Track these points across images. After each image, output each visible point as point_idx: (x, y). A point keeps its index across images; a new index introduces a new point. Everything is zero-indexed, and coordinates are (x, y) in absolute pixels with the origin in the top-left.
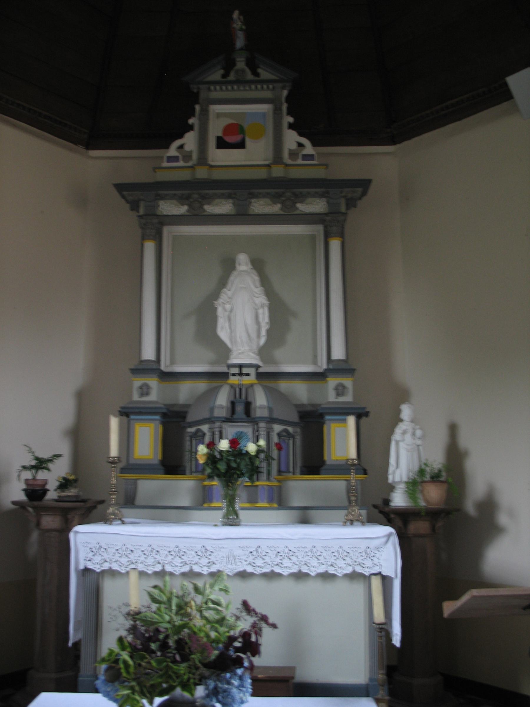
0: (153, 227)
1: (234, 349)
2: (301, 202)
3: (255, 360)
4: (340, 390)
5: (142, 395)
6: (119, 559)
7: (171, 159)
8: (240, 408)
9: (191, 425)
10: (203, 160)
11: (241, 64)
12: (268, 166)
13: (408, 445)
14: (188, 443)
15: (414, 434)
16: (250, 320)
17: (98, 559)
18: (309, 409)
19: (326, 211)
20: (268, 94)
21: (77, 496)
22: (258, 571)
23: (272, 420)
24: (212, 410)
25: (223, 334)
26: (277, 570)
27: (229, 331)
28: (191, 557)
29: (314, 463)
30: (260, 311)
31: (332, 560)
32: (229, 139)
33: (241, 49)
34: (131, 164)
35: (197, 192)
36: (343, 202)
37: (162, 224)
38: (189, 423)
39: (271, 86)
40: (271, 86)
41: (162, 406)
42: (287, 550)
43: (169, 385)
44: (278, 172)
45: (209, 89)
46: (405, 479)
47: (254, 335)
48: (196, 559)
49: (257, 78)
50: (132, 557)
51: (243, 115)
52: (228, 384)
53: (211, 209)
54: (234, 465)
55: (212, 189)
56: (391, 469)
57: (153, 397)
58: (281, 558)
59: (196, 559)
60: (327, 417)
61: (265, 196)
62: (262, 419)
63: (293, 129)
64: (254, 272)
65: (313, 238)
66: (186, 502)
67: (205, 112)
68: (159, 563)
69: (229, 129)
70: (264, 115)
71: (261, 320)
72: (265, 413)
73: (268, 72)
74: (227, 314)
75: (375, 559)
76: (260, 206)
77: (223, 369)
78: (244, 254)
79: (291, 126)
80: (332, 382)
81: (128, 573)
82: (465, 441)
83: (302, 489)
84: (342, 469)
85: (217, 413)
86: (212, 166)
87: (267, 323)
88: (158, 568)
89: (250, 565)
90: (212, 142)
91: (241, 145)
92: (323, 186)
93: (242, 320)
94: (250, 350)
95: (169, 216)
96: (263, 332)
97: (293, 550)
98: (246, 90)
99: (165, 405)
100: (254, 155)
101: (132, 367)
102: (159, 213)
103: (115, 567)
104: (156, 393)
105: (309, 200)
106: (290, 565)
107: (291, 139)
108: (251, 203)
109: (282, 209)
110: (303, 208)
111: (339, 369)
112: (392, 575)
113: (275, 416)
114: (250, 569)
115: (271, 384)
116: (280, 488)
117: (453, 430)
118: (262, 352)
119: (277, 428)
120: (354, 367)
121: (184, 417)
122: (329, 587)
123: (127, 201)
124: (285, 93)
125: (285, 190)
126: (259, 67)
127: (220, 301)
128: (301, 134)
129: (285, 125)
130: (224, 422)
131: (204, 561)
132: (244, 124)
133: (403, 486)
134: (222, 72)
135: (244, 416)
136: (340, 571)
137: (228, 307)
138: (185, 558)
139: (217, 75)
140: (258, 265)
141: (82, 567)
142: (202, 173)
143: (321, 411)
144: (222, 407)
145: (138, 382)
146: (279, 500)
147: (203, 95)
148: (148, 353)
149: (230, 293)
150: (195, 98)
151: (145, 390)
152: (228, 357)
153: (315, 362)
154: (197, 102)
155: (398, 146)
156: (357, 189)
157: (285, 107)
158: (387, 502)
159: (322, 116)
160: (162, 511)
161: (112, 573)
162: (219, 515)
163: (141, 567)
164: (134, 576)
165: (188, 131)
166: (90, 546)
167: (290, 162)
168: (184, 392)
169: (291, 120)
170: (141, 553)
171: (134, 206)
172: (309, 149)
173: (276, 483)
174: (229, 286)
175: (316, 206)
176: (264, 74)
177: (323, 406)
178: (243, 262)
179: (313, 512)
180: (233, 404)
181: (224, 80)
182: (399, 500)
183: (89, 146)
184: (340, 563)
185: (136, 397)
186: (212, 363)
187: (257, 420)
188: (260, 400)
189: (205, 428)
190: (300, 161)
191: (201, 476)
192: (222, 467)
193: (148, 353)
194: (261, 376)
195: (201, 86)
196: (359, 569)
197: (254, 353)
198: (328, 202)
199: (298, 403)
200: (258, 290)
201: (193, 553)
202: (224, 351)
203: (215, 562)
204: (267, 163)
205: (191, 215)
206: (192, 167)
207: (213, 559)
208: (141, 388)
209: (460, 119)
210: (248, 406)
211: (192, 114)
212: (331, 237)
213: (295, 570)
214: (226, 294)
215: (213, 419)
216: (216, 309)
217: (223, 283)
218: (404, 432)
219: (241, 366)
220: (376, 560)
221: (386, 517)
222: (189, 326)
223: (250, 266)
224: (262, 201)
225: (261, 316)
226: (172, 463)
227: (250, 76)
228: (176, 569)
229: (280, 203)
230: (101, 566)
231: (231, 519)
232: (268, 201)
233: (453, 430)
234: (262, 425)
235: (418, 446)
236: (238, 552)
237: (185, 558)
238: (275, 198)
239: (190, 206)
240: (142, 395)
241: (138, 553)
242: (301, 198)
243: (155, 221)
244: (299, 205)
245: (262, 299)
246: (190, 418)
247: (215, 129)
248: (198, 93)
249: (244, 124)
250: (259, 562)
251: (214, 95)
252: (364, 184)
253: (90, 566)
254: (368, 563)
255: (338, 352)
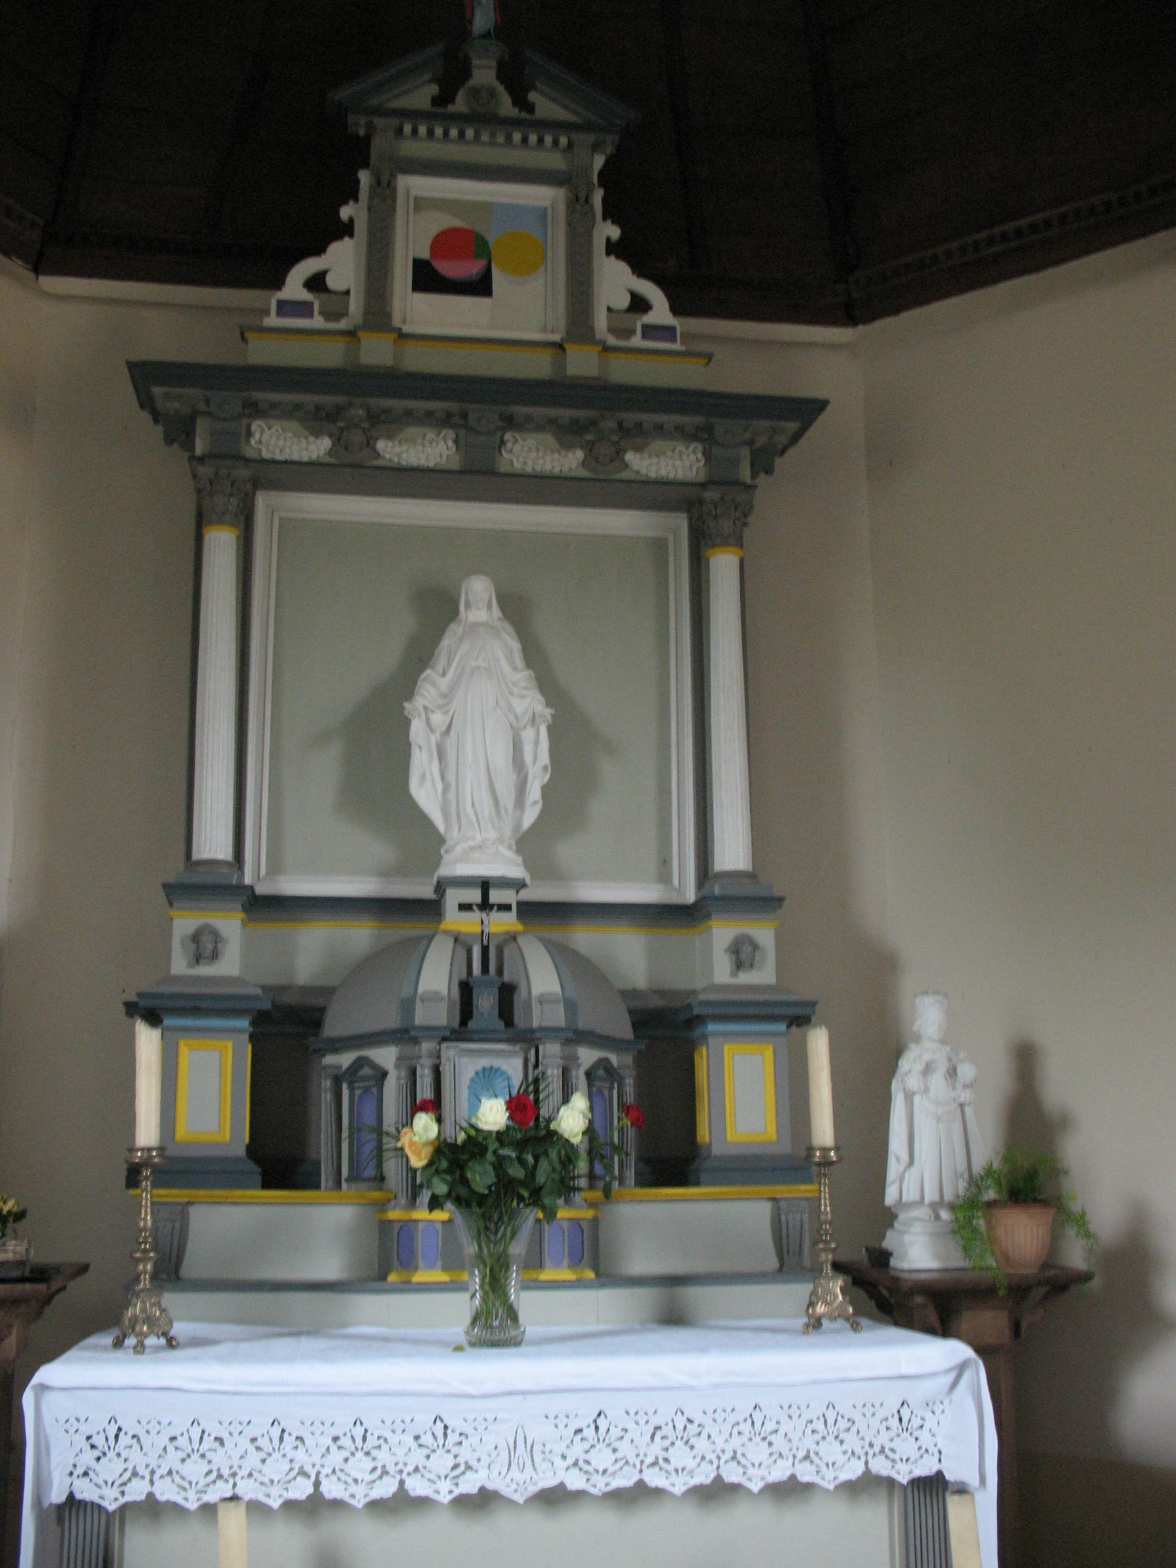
0: (229, 489)
1: (453, 836)
2: (638, 449)
3: (515, 870)
4: (743, 954)
5: (198, 959)
6: (177, 1466)
7: (286, 308)
8: (486, 1003)
9: (339, 1045)
10: (378, 314)
11: (484, 74)
12: (560, 346)
13: (938, 1104)
14: (327, 1097)
15: (952, 1073)
16: (501, 758)
17: (110, 1469)
18: (656, 1002)
19: (702, 478)
20: (555, 161)
21: (20, 1264)
22: (599, 1485)
23: (576, 1036)
24: (408, 1005)
25: (425, 792)
26: (654, 1479)
27: (439, 786)
28: (400, 1452)
29: (670, 1153)
30: (528, 735)
31: (809, 1442)
32: (450, 269)
33: (486, 35)
34: (170, 318)
35: (358, 401)
36: (745, 453)
37: (257, 484)
38: (332, 1041)
39: (563, 141)
40: (563, 141)
41: (259, 991)
42: (680, 1422)
43: (270, 931)
44: (582, 363)
45: (400, 131)
46: (931, 1195)
47: (508, 799)
48: (417, 1457)
49: (524, 115)
50: (220, 1459)
51: (487, 208)
52: (446, 932)
53: (394, 450)
54: (516, 1172)
55: (401, 397)
56: (893, 1169)
57: (229, 965)
58: (667, 1443)
59: (417, 1457)
60: (711, 1027)
61: (541, 427)
62: (551, 1032)
63: (619, 256)
64: (509, 627)
65: (659, 547)
66: (330, 1268)
67: (385, 190)
68: (303, 1473)
69: (446, 242)
70: (542, 215)
71: (528, 758)
72: (557, 1017)
73: (554, 100)
74: (434, 739)
75: (924, 1435)
76: (527, 453)
77: (426, 891)
78: (482, 577)
79: (612, 249)
80: (722, 932)
81: (209, 1510)
82: (1059, 1087)
83: (651, 1225)
84: (750, 1169)
85: (422, 1016)
86: (402, 336)
87: (545, 768)
88: (301, 1490)
89: (576, 1470)
90: (402, 275)
91: (481, 287)
92: (704, 413)
93: (478, 759)
94: (500, 840)
95: (280, 462)
96: (534, 792)
97: (698, 1418)
98: (499, 145)
99: (264, 988)
100: (516, 315)
101: (171, 879)
102: (250, 453)
103: (166, 1492)
104: (239, 954)
105: (658, 444)
106: (691, 1464)
107: (615, 281)
108: (503, 442)
109: (584, 464)
110: (645, 464)
111: (716, 897)
112: (973, 1480)
113: (582, 1024)
114: (575, 1482)
115: (557, 934)
116: (595, 1221)
117: (1026, 1060)
118: (528, 844)
119: (587, 1056)
120: (778, 892)
121: (317, 1024)
122: (795, 1519)
123: (157, 417)
124: (599, 161)
125: (600, 413)
126: (534, 88)
127: (419, 702)
128: (639, 270)
129: (599, 246)
130: (445, 1039)
131: (442, 1463)
132: (486, 232)
133: (923, 1212)
134: (434, 89)
135: (500, 1025)
136: (829, 1474)
137: (438, 719)
138: (383, 1456)
139: (421, 96)
140: (515, 609)
141: (57, 1496)
142: (376, 351)
143: (696, 1011)
144: (435, 997)
145: (185, 923)
146: (596, 1261)
147: (378, 145)
148: (213, 841)
149: (444, 683)
150: (358, 152)
151: (205, 946)
152: (437, 861)
153: (664, 877)
154: (366, 165)
155: (861, 328)
156: (783, 424)
157: (598, 196)
158: (881, 1258)
159: (692, 227)
160: (272, 1301)
161: (153, 1509)
162: (458, 1309)
163: (248, 1490)
164: (233, 1521)
165: (339, 237)
166: (86, 1429)
167: (612, 340)
168: (310, 954)
169: (615, 232)
170: (251, 1448)
171: (179, 431)
172: (661, 312)
173: (589, 1214)
174: (442, 662)
175: (675, 462)
176: (546, 106)
177: (703, 997)
178: (479, 598)
179: (695, 1294)
180: (466, 989)
181: (441, 110)
182: (918, 1252)
183: (39, 265)
184: (831, 1451)
185: (179, 965)
186: (385, 873)
187: (538, 1035)
188: (541, 978)
189: (386, 1056)
190: (637, 341)
191: (377, 1195)
192: (481, 1177)
193: (213, 841)
194: (531, 911)
195: (378, 122)
196: (880, 1467)
197: (509, 848)
198: (707, 455)
199: (629, 986)
200: (522, 677)
201: (408, 1439)
202: (421, 839)
203: (473, 1463)
204: (556, 338)
205: (335, 465)
206: (351, 334)
207: (465, 1454)
208: (196, 937)
209: (1037, 269)
210: (507, 993)
211: (352, 194)
212: (714, 546)
213: (704, 1476)
214: (434, 684)
215: (413, 1033)
216: (407, 723)
217: (420, 655)
218: (928, 1069)
219: (485, 885)
220: (925, 1438)
221: (871, 1296)
222: (323, 772)
223: (496, 612)
224: (531, 440)
225: (528, 750)
226: (278, 1158)
227: (506, 107)
228: (353, 1489)
229: (582, 447)
230: (123, 1493)
231: (495, 1327)
232: (548, 438)
233: (1026, 1060)
234: (551, 1050)
235: (962, 1106)
236: (539, 1432)
237: (383, 1456)
238: (569, 434)
239: (337, 440)
240: (739, 965)
241: (237, 1446)
242: (636, 436)
243: (242, 473)
244: (629, 456)
245: (530, 703)
246: (333, 1027)
247: (412, 240)
248: (367, 139)
249: (486, 232)
250: (602, 1458)
251: (410, 148)
252: (808, 410)
253: (86, 1491)
254: (905, 1446)
255: (733, 852)
